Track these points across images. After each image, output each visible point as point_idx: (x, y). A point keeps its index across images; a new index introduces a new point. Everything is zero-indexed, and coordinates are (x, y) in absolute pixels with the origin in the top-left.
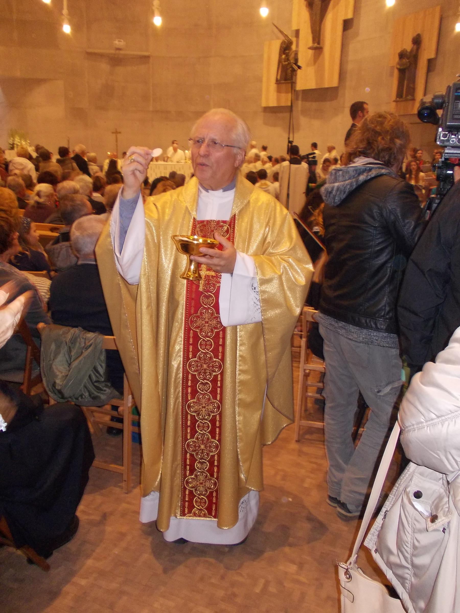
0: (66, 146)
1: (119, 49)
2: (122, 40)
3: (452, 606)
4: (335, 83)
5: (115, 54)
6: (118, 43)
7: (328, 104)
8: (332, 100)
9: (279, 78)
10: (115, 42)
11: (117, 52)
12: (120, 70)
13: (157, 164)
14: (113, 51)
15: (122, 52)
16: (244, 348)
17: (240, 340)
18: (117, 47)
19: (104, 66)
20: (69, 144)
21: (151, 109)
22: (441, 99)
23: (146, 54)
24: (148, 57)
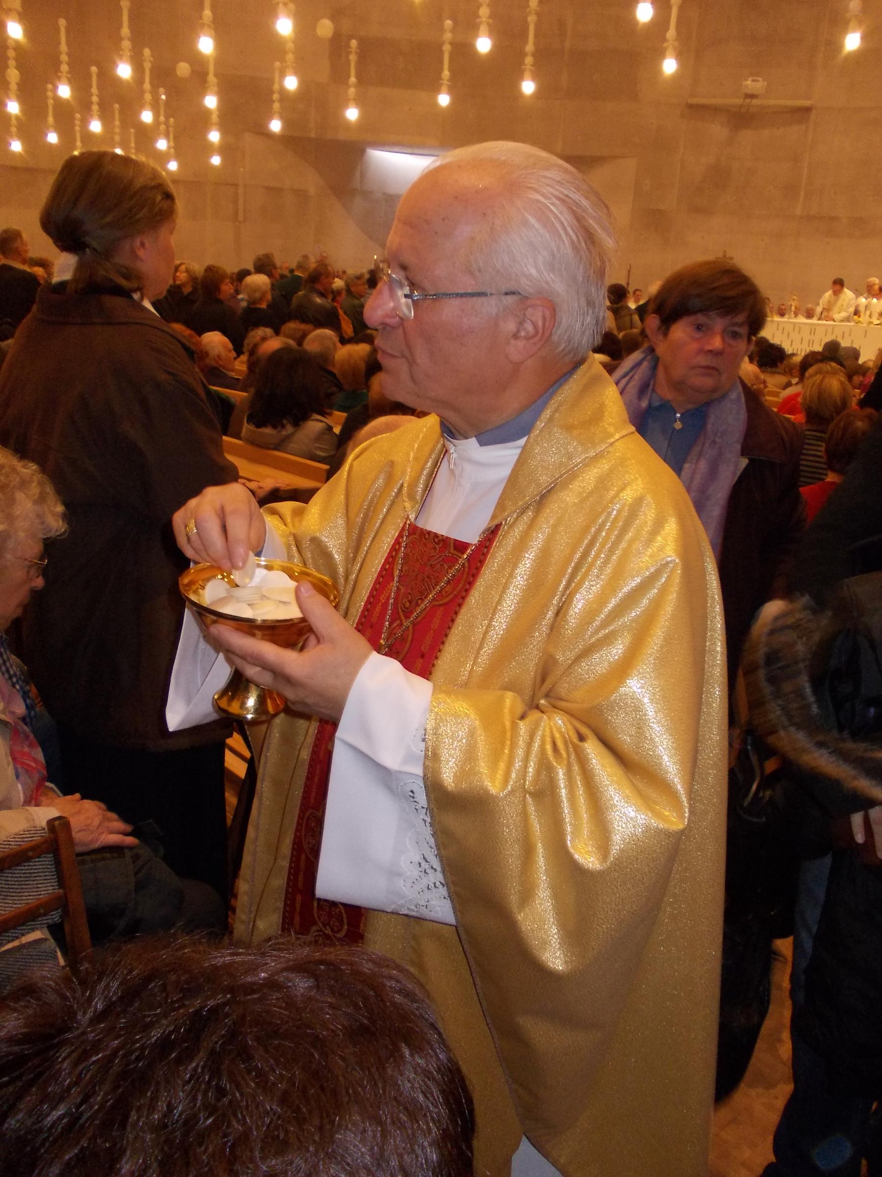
0: (623, 283)
1: (752, 96)
2: (760, 79)
3: (421, 156)
5: (741, 106)
6: (751, 84)
10: (744, 83)
11: (748, 100)
12: (747, 137)
13: (797, 323)
14: (738, 101)
15: (755, 102)
16: (183, 979)
17: (260, 1157)
18: (750, 92)
19: (718, 130)
20: (628, 284)
21: (799, 211)
22: (348, 1132)
23: (807, 103)
24: (808, 110)
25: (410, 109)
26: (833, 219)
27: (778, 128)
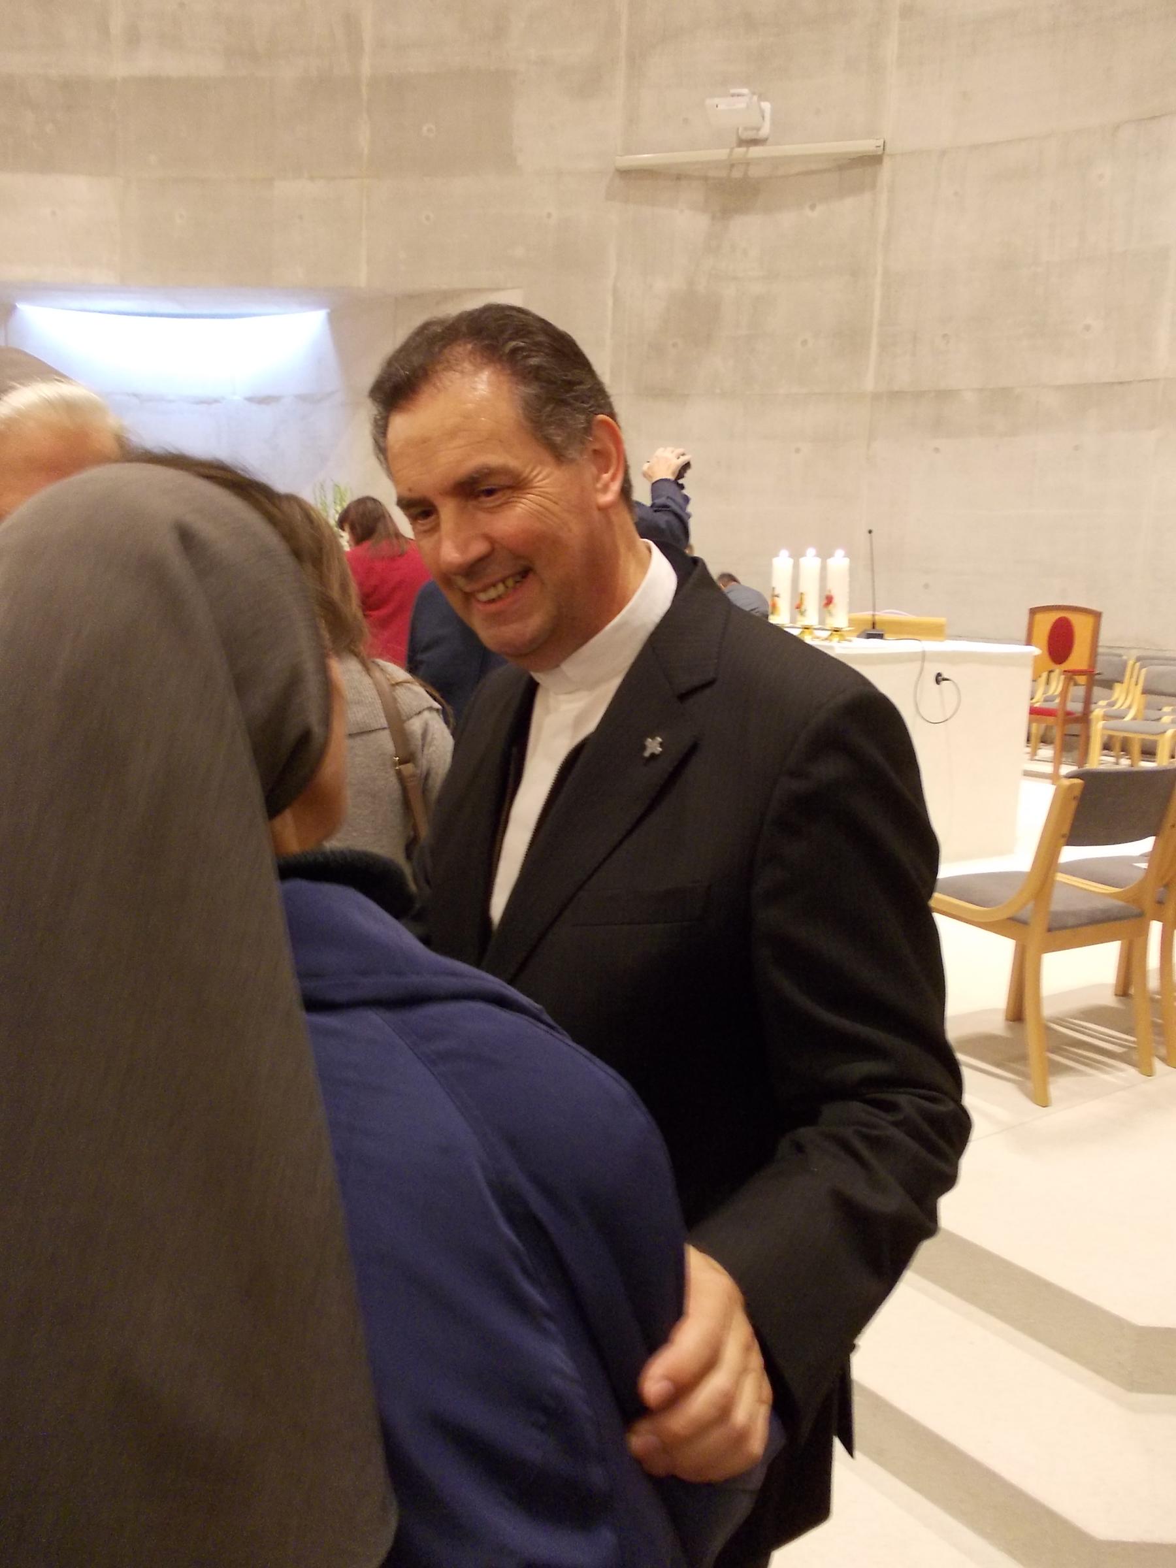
2: (745, 91)
14: (721, 154)
15: (755, 152)
21: (869, 384)
23: (867, 145)
24: (873, 160)
25: (54, 213)
26: (944, 395)
27: (813, 207)
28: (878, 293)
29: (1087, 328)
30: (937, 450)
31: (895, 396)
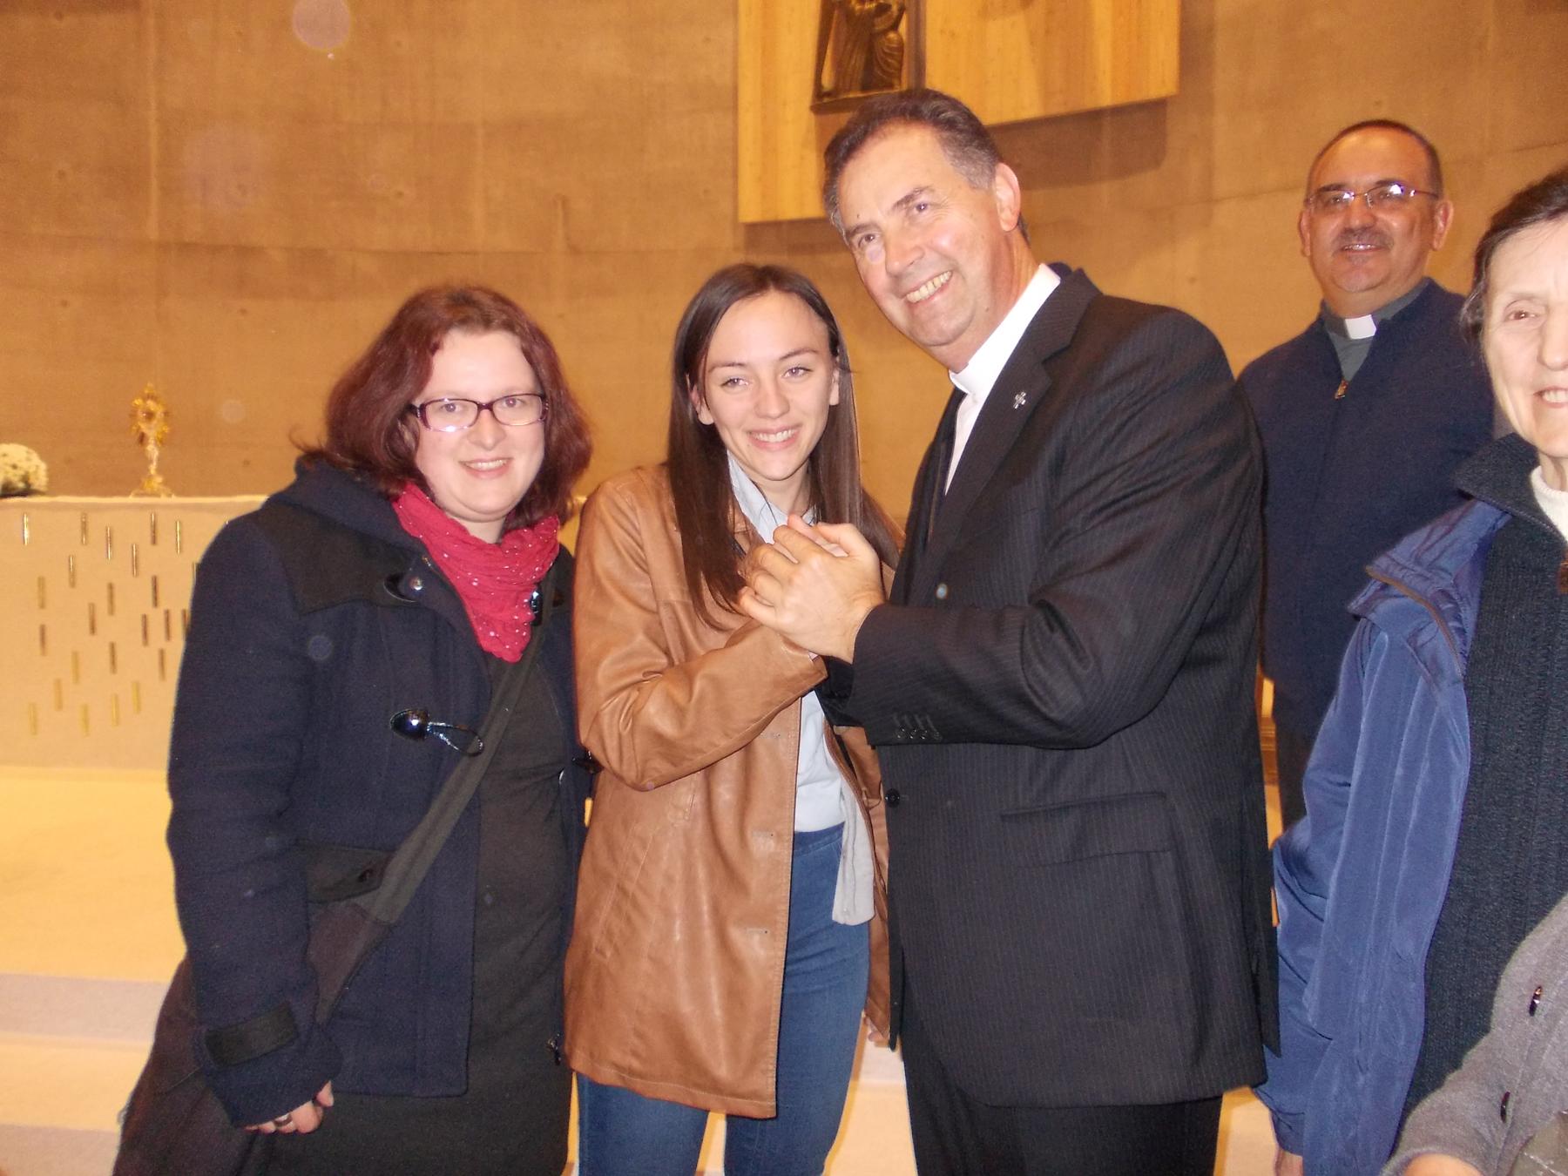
4: (1160, 78)
7: (1105, 191)
8: (1123, 170)
9: (827, 81)
21: (152, 231)
26: (246, 252)
27: (59, 16)
28: (154, 129)
29: (400, 194)
30: (243, 312)
31: (186, 248)
